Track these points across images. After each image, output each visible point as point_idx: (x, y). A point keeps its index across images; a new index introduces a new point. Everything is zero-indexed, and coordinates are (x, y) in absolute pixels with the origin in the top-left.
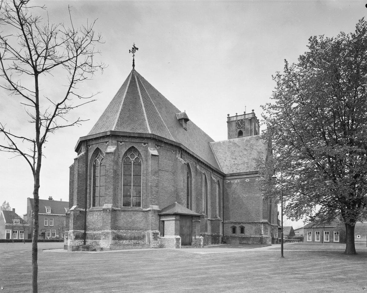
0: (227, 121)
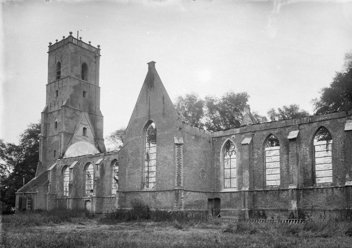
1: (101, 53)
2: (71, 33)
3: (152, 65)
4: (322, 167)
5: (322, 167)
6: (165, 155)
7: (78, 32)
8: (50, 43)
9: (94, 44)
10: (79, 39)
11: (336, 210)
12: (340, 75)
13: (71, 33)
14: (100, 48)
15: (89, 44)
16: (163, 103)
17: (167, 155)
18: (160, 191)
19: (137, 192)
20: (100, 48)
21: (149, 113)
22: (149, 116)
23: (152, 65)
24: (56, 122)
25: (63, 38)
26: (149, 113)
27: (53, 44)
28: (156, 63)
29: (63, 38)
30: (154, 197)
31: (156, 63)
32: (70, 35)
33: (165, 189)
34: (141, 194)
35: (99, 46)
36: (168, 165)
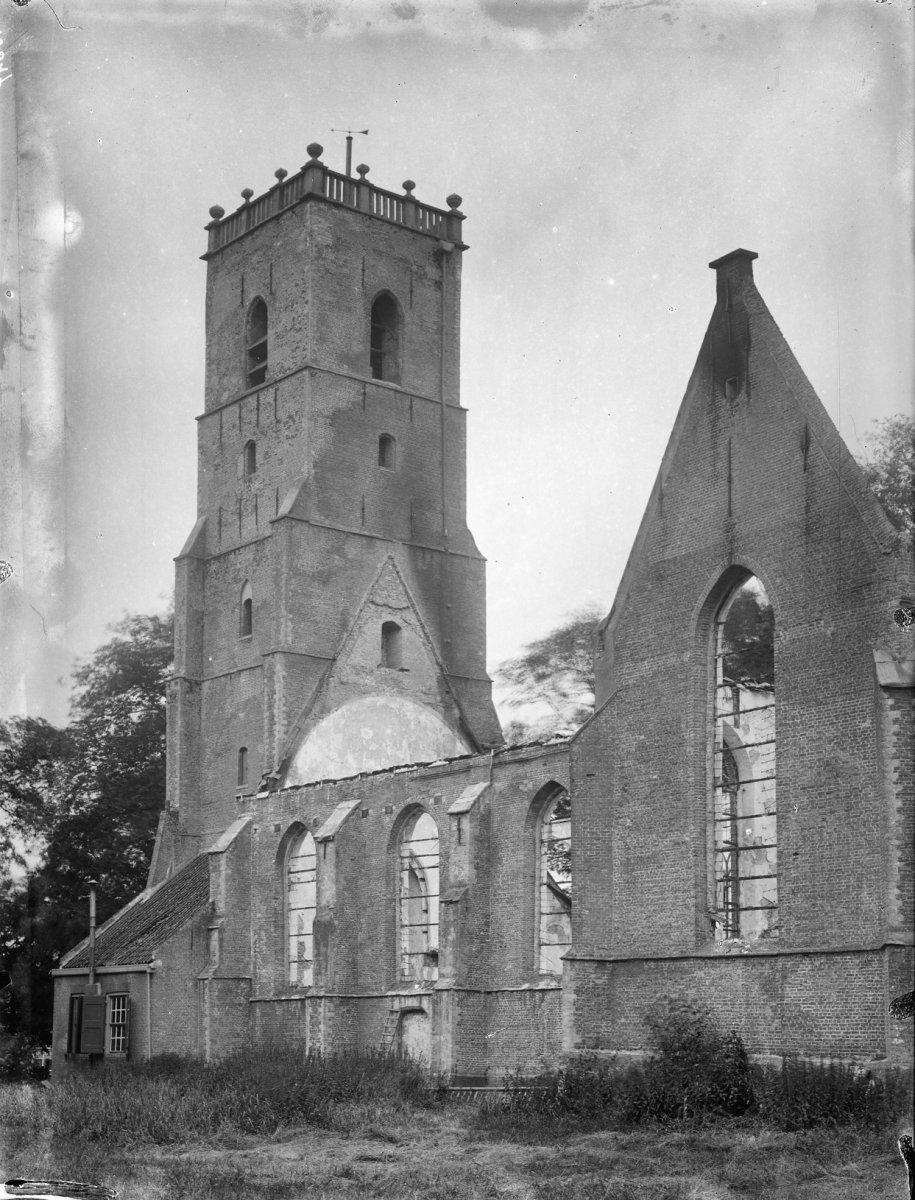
0: (204, 250)
1: (468, 232)
2: (315, 150)
3: (734, 269)
7: (349, 139)
8: (216, 212)
9: (431, 195)
10: (356, 176)
13: (315, 150)
14: (459, 209)
15: (403, 192)
18: (806, 955)
19: (678, 964)
20: (459, 209)
24: (249, 602)
25: (276, 181)
27: (229, 212)
29: (276, 181)
32: (309, 158)
33: (836, 945)
35: (454, 201)
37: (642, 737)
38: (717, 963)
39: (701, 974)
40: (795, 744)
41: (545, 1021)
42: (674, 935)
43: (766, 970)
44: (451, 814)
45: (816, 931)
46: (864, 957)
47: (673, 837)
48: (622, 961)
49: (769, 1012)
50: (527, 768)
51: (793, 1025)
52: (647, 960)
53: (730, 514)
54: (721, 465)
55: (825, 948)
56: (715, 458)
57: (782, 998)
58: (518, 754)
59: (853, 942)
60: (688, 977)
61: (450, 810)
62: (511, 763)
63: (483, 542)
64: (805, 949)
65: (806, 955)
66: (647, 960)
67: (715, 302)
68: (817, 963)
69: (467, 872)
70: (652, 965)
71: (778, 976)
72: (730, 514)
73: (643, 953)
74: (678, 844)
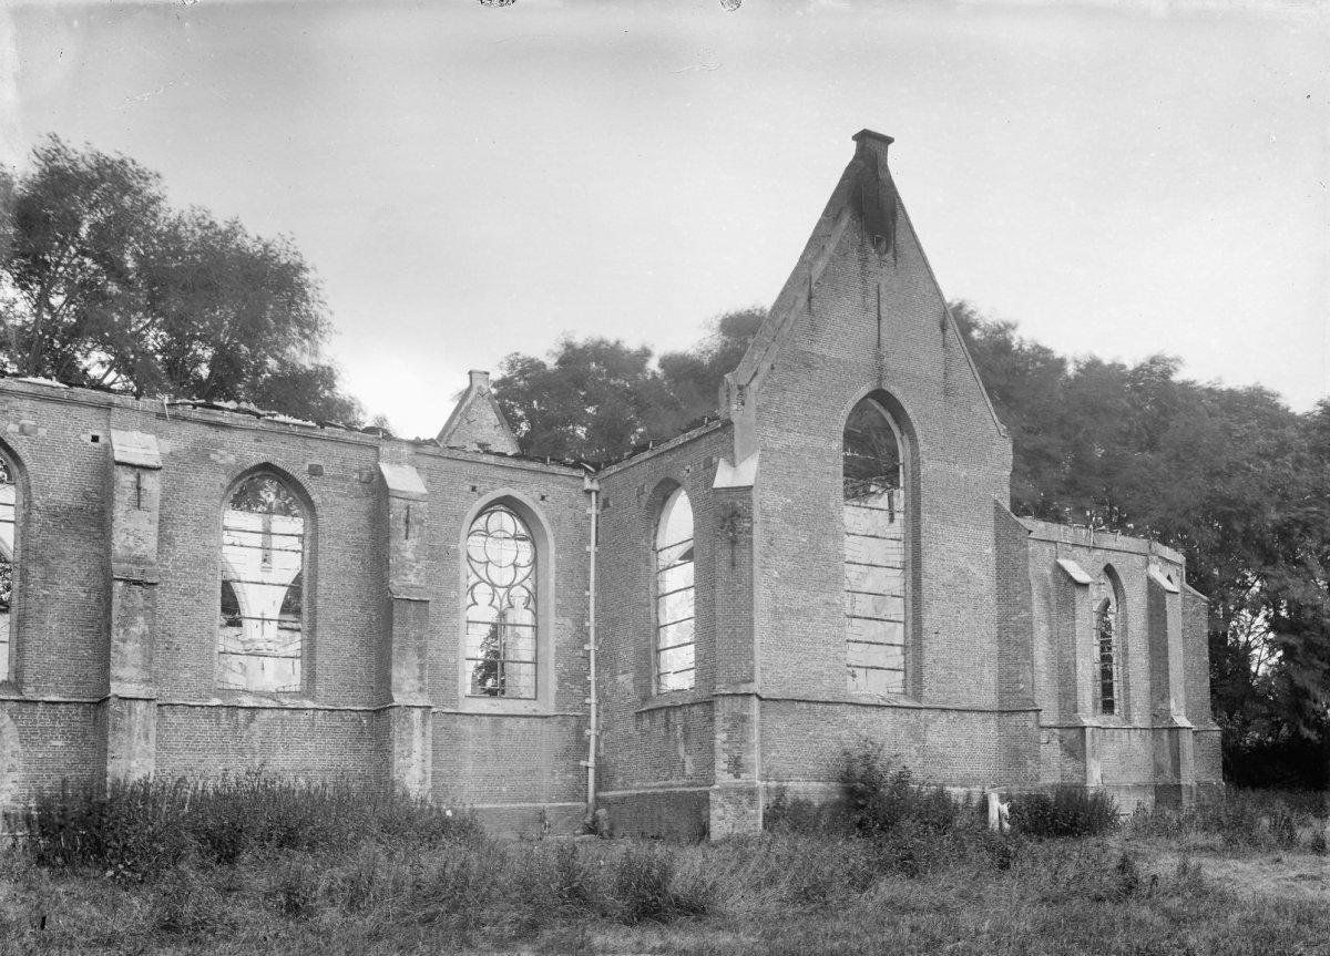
3: (871, 148)
4: (879, 656)
5: (879, 656)
6: (962, 562)
11: (1138, 787)
12: (234, 230)
16: (944, 345)
17: (971, 567)
18: (943, 710)
19: (830, 707)
21: (879, 357)
22: (880, 369)
23: (871, 148)
26: (879, 357)
28: (889, 140)
30: (916, 735)
31: (889, 140)
33: (964, 705)
34: (851, 717)
36: (972, 605)
37: (789, 500)
38: (868, 710)
39: (853, 717)
40: (936, 549)
41: (257, 745)
42: (826, 682)
43: (912, 719)
44: (1060, 568)
45: (951, 693)
46: (985, 715)
47: (826, 597)
48: (771, 700)
49: (914, 752)
50: (223, 435)
51: (933, 762)
52: (799, 701)
53: (879, 346)
54: (871, 301)
55: (956, 706)
56: (865, 294)
57: (924, 741)
58: (215, 415)
59: (976, 704)
60: (840, 719)
61: (1063, 562)
62: (196, 421)
63: (1126, 351)
64: (944, 706)
65: (943, 710)
66: (799, 701)
67: (850, 158)
68: (951, 717)
69: (117, 548)
70: (804, 705)
71: (922, 724)
72: (879, 346)
73: (800, 694)
74: (828, 603)
